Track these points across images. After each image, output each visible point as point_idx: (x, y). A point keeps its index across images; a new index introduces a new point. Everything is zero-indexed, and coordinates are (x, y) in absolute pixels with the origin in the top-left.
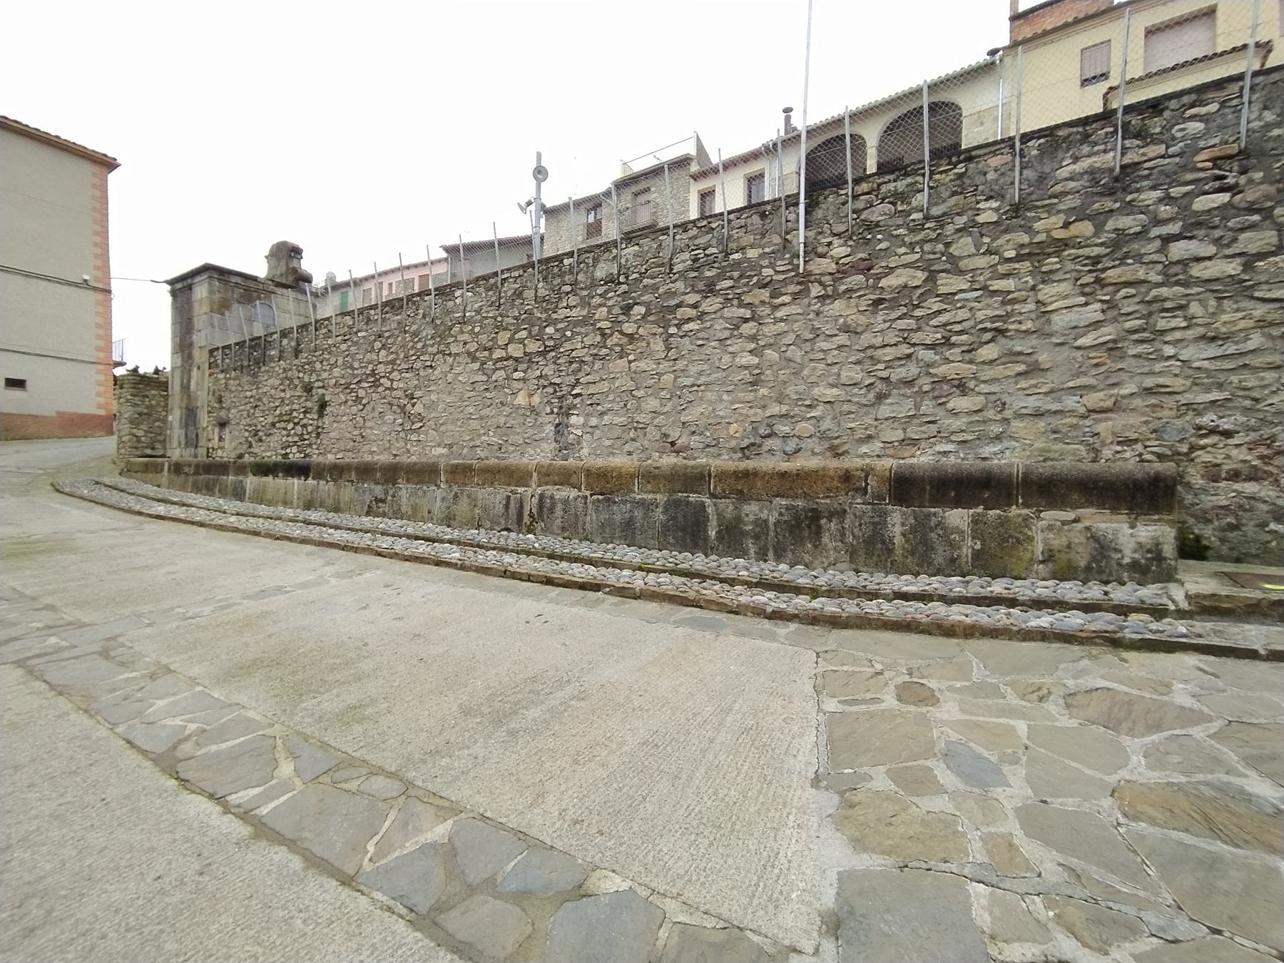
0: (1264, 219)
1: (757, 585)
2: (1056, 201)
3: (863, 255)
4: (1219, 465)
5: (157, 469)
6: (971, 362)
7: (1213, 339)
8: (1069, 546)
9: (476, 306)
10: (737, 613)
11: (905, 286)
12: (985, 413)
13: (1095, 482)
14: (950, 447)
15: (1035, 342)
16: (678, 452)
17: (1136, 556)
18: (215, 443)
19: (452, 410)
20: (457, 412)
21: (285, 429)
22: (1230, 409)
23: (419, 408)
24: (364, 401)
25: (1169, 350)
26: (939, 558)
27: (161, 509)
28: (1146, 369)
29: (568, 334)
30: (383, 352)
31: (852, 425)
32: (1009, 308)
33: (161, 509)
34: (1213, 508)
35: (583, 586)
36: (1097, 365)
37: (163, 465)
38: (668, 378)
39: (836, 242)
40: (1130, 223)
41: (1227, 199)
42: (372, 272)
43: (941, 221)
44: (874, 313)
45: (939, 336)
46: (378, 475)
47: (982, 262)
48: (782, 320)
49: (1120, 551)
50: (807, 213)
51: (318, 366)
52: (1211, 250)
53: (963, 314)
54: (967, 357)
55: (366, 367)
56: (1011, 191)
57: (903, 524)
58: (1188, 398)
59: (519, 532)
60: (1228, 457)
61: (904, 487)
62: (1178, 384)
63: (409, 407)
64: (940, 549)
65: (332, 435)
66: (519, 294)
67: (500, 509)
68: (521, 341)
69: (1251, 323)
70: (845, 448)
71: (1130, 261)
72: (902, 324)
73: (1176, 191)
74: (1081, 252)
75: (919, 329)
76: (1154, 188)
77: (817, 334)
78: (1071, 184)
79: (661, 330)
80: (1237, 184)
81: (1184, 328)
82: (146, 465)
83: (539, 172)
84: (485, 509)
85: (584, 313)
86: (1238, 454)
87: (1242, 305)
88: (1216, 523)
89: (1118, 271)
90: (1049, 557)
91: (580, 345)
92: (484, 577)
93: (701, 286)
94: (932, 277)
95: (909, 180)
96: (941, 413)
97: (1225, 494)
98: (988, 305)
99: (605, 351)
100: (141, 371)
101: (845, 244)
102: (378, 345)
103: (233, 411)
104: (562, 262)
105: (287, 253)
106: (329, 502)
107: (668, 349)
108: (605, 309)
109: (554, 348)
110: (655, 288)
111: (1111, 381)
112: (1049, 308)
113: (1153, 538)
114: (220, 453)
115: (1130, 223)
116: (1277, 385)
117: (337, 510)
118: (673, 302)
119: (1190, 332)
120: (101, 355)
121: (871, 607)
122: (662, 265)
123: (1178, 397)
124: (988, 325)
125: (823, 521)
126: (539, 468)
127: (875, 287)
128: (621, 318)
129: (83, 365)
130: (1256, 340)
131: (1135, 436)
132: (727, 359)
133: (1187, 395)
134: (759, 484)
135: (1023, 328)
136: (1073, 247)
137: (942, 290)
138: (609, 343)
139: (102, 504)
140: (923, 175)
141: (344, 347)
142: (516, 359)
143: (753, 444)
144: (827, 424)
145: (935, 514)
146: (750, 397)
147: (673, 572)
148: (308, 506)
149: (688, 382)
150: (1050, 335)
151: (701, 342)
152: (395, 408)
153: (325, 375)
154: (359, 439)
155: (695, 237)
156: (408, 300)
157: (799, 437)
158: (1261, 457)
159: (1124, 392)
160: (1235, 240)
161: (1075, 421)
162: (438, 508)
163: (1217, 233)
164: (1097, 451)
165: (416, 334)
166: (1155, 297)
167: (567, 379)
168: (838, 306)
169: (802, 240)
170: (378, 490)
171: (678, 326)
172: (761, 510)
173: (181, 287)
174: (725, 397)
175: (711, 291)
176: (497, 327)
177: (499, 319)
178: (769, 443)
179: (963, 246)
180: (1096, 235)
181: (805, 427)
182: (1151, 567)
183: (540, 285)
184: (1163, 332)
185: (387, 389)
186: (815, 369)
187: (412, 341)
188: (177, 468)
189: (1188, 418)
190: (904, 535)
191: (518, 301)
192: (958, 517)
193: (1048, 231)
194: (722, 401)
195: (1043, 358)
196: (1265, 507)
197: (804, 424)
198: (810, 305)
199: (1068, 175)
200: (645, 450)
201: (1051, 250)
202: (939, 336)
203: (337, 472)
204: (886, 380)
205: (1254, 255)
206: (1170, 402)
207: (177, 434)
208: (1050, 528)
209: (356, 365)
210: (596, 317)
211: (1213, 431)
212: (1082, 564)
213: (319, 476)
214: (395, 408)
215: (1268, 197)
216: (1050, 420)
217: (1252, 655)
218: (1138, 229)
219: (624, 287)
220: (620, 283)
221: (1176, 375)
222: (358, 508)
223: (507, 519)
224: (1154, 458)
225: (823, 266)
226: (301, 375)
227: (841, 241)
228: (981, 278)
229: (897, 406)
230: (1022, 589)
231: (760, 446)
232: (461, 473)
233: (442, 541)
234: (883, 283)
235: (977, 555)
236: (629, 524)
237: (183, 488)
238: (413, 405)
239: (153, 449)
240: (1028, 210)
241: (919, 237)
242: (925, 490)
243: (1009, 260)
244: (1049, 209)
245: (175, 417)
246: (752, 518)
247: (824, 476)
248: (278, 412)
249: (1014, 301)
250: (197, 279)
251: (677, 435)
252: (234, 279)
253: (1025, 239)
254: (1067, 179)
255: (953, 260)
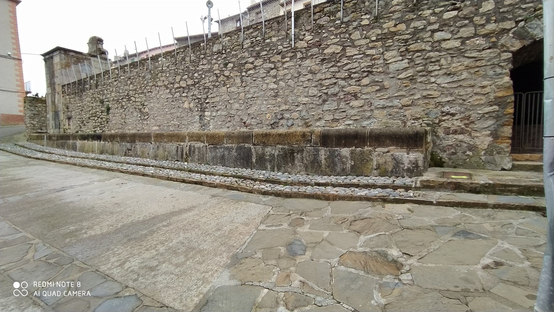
0: (470, 22)
1: (265, 181)
2: (392, 15)
3: (317, 39)
4: (450, 128)
5: (42, 138)
6: (359, 85)
7: (449, 74)
8: (385, 163)
9: (167, 65)
10: (251, 193)
11: (334, 53)
12: (364, 107)
13: (395, 135)
14: (351, 122)
15: (383, 77)
16: (246, 127)
17: (409, 166)
18: (67, 126)
19: (159, 110)
20: (164, 111)
21: (94, 120)
22: (454, 104)
23: (146, 110)
24: (125, 107)
25: (433, 80)
26: (338, 169)
27: (39, 155)
28: (424, 88)
29: (203, 76)
30: (131, 86)
31: (313, 113)
32: (373, 62)
33: (39, 155)
34: (447, 146)
35: (196, 183)
36: (406, 86)
37: (44, 136)
38: (242, 95)
39: (307, 34)
40: (419, 24)
41: (456, 14)
42: (145, 49)
43: (348, 24)
44: (322, 65)
45: (347, 74)
46: (128, 139)
47: (363, 42)
48: (286, 69)
49: (403, 164)
50: (295, 21)
51: (105, 92)
52: (449, 36)
53: (356, 65)
54: (358, 83)
55: (125, 92)
56: (374, 10)
57: (325, 155)
58: (439, 100)
59: (182, 161)
60: (453, 124)
61: (326, 139)
62: (436, 94)
63: (143, 109)
64: (339, 165)
65: (113, 122)
66: (183, 59)
67: (174, 152)
68: (185, 80)
69: (463, 67)
70: (311, 123)
71: (419, 41)
72: (332, 69)
73: (437, 10)
74: (401, 37)
75: (339, 72)
76: (429, 9)
77: (300, 74)
78: (398, 7)
79: (239, 74)
80: (460, 7)
81: (439, 70)
82: (37, 136)
83: (209, 3)
84: (169, 152)
85: (209, 67)
86: (457, 124)
87: (460, 60)
88: (448, 152)
89: (414, 45)
90: (378, 167)
91: (208, 81)
92: (160, 180)
93: (254, 54)
94: (344, 49)
95: (335, 6)
96: (347, 107)
97: (451, 140)
98: (366, 61)
99: (217, 83)
100: (40, 96)
101: (310, 35)
102: (129, 82)
103: (73, 112)
104: (200, 45)
105: (96, 42)
106: (110, 151)
107: (242, 82)
108: (217, 65)
109: (198, 82)
110: (236, 55)
111: (410, 93)
112: (388, 62)
113: (415, 158)
114: (69, 131)
115: (419, 24)
116: (472, 94)
117: (113, 154)
118: (244, 62)
119: (441, 72)
120: (19, 88)
121: (303, 189)
122: (239, 45)
123: (435, 99)
124: (365, 69)
125: (295, 154)
126: (189, 134)
127: (322, 53)
128: (224, 69)
129: (10, 93)
130: (465, 75)
131: (419, 116)
132: (265, 86)
133: (439, 99)
134: (271, 139)
135: (379, 71)
136: (398, 35)
137: (348, 54)
138: (219, 80)
139: (15, 154)
140: (340, 4)
141: (115, 83)
142: (183, 88)
143: (275, 122)
144: (304, 113)
145: (337, 150)
146: (274, 102)
147: (234, 177)
148: (102, 153)
149: (250, 96)
150: (389, 73)
151: (255, 79)
152: (137, 110)
153: (109, 96)
154: (124, 123)
155: (252, 33)
156: (140, 62)
157: (293, 119)
158: (465, 124)
159: (415, 98)
160: (458, 31)
161: (397, 110)
162: (151, 152)
163: (452, 29)
164: (405, 123)
165: (144, 77)
166: (428, 57)
167: (203, 96)
168: (307, 62)
169: (293, 33)
170: (128, 145)
171: (246, 72)
172: (272, 150)
173: (48, 57)
174: (264, 102)
175: (258, 56)
176: (175, 74)
177: (176, 70)
178: (282, 121)
179: (356, 35)
180: (407, 30)
181: (296, 115)
182: (414, 170)
183: (192, 55)
184: (431, 72)
185: (134, 102)
186: (299, 89)
187: (142, 80)
188: (50, 138)
189: (439, 108)
190: (325, 159)
191: (183, 62)
192: (345, 151)
193: (388, 28)
194: (263, 104)
195: (386, 83)
196: (465, 145)
197: (295, 113)
198: (297, 62)
199: (396, 3)
200: (234, 126)
201: (389, 37)
202: (347, 74)
203: (112, 138)
204: (326, 94)
205: (465, 38)
206: (432, 101)
207: (51, 123)
208: (379, 155)
209: (121, 91)
210: (214, 68)
211: (448, 114)
212: (390, 170)
213: (105, 140)
214: (137, 110)
215: (471, 12)
216: (388, 110)
217: (431, 203)
218: (422, 27)
219: (225, 55)
220: (223, 54)
221: (435, 90)
222: (121, 153)
223: (177, 156)
224: (425, 125)
225: (302, 44)
226: (99, 96)
227: (309, 33)
228: (363, 49)
229: (331, 105)
230: (370, 180)
231: (278, 123)
232: (159, 137)
233: (149, 166)
234: (325, 51)
235: (352, 167)
236: (223, 157)
237: (52, 146)
238: (144, 109)
239: (41, 129)
240: (381, 19)
241: (339, 32)
242: (333, 140)
243: (373, 41)
244: (389, 18)
245: (50, 116)
246: (268, 153)
247: (295, 135)
248: (91, 113)
249: (375, 59)
250: (55, 54)
251: (246, 119)
252: (71, 54)
253: (379, 32)
254: (396, 5)
255: (352, 41)
